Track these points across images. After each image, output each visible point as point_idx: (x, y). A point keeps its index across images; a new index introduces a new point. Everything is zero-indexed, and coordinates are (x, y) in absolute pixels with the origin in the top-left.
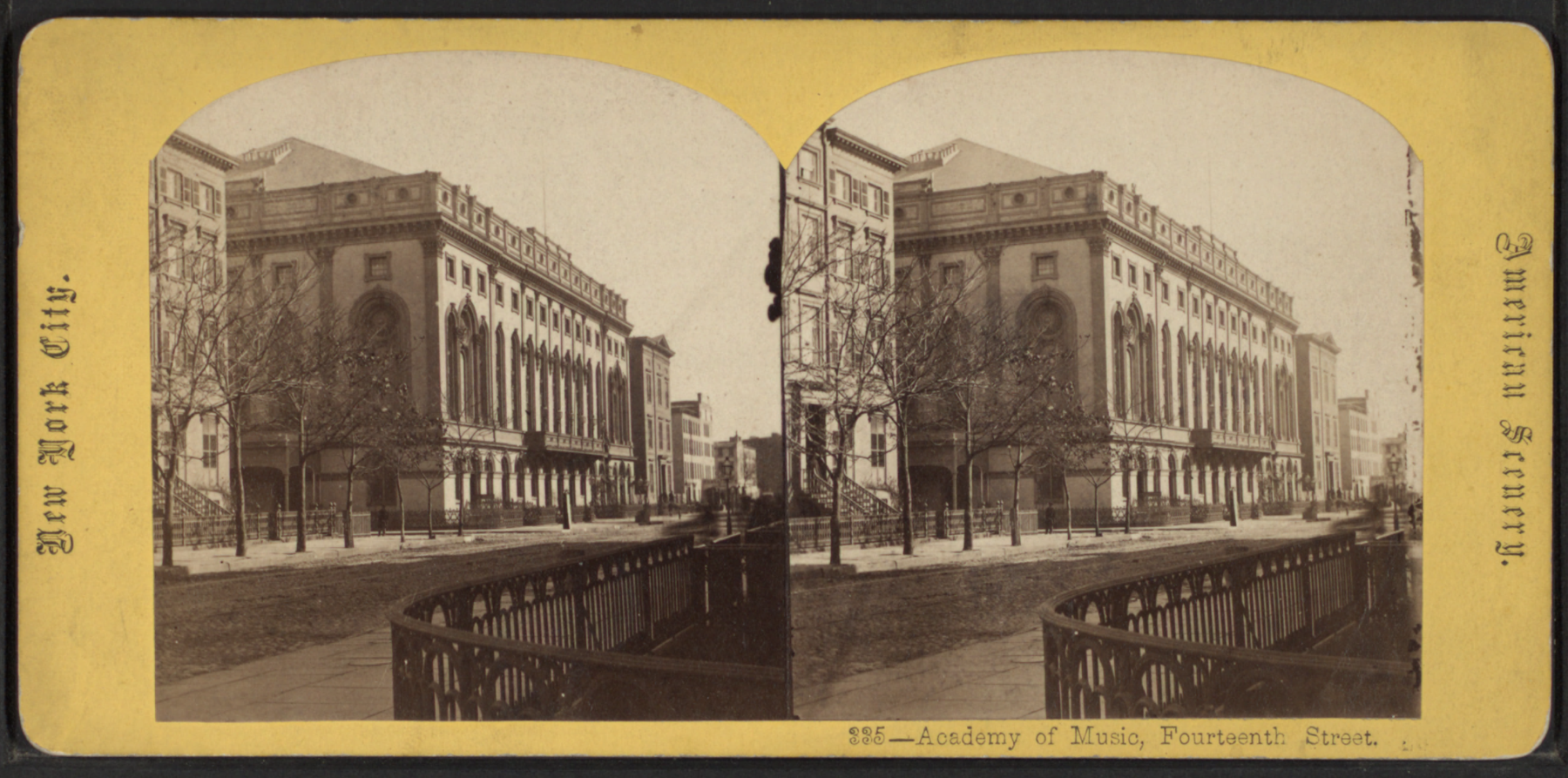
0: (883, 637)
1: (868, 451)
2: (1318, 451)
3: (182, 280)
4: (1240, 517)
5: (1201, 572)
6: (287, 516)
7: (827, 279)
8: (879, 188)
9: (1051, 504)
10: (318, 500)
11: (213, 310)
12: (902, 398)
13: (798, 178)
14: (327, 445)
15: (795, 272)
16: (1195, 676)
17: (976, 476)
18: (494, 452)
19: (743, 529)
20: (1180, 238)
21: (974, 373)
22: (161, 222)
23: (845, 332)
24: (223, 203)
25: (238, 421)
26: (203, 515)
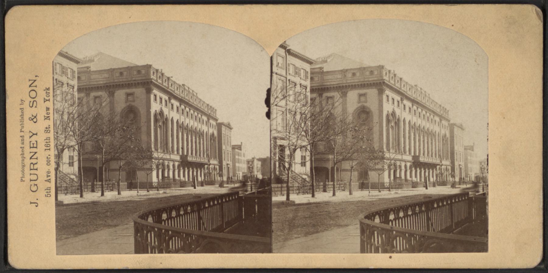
0: (304, 226)
1: (68, 161)
2: (456, 164)
4: (429, 186)
5: (187, 205)
6: (98, 184)
7: (286, 101)
10: (340, 178)
11: (72, 112)
12: (312, 143)
13: (277, 66)
14: (112, 159)
15: (275, 99)
16: (412, 241)
17: (105, 171)
19: (256, 190)
20: (410, 89)
21: (105, 134)
22: (288, 82)
23: (292, 119)
26: (69, 183)
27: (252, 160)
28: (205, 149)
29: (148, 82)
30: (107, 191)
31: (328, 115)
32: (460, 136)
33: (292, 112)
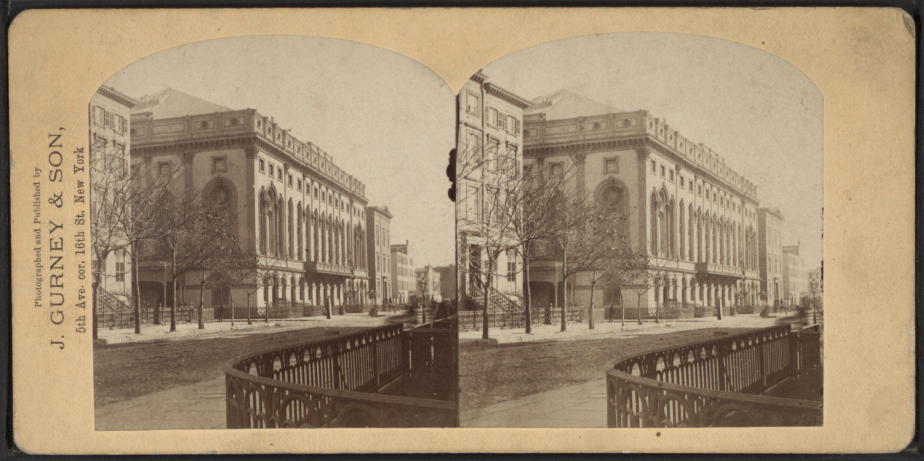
1: (114, 272)
2: (770, 276)
3: (496, 172)
4: (724, 314)
6: (165, 310)
7: (483, 171)
8: (121, 117)
9: (612, 305)
11: (122, 189)
12: (135, 241)
13: (467, 111)
14: (188, 269)
15: (464, 167)
17: (178, 288)
18: (286, 273)
19: (432, 320)
20: (691, 150)
22: (485, 138)
23: (493, 202)
24: (129, 128)
25: (136, 254)
26: (116, 310)
27: (425, 270)
28: (346, 251)
29: (249, 139)
30: (181, 322)
31: (553, 195)
32: (775, 230)
33: (492, 190)
